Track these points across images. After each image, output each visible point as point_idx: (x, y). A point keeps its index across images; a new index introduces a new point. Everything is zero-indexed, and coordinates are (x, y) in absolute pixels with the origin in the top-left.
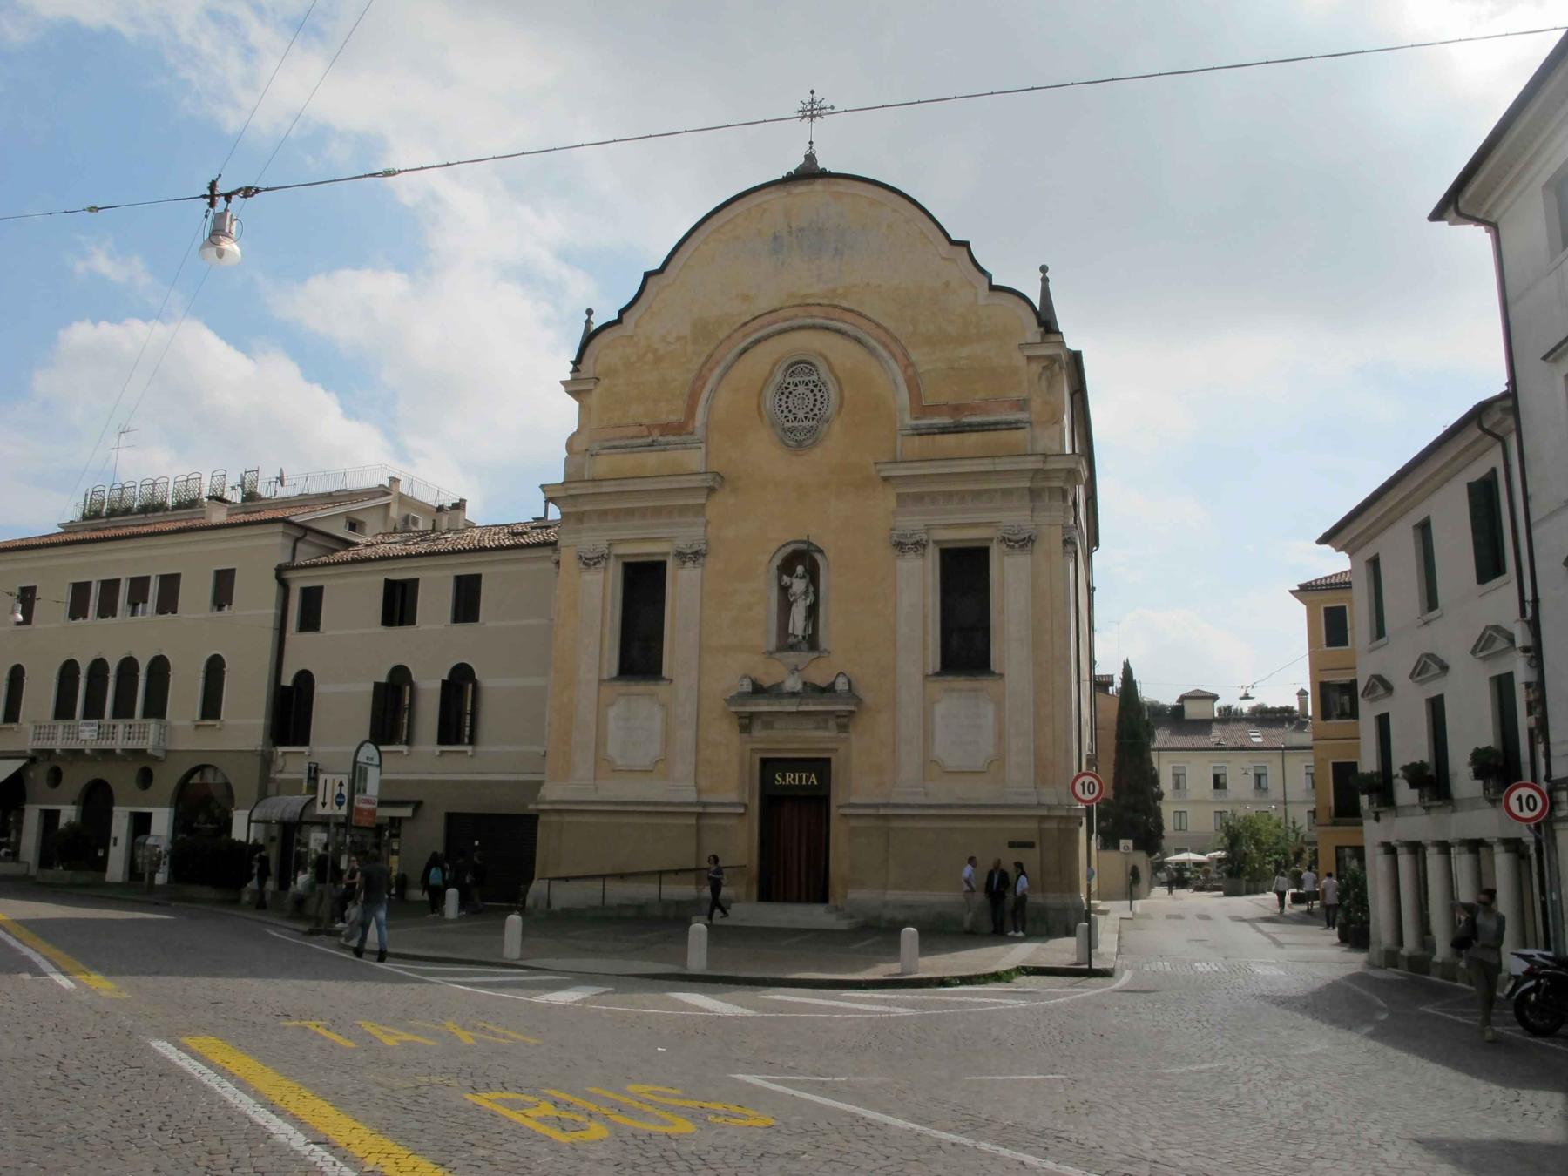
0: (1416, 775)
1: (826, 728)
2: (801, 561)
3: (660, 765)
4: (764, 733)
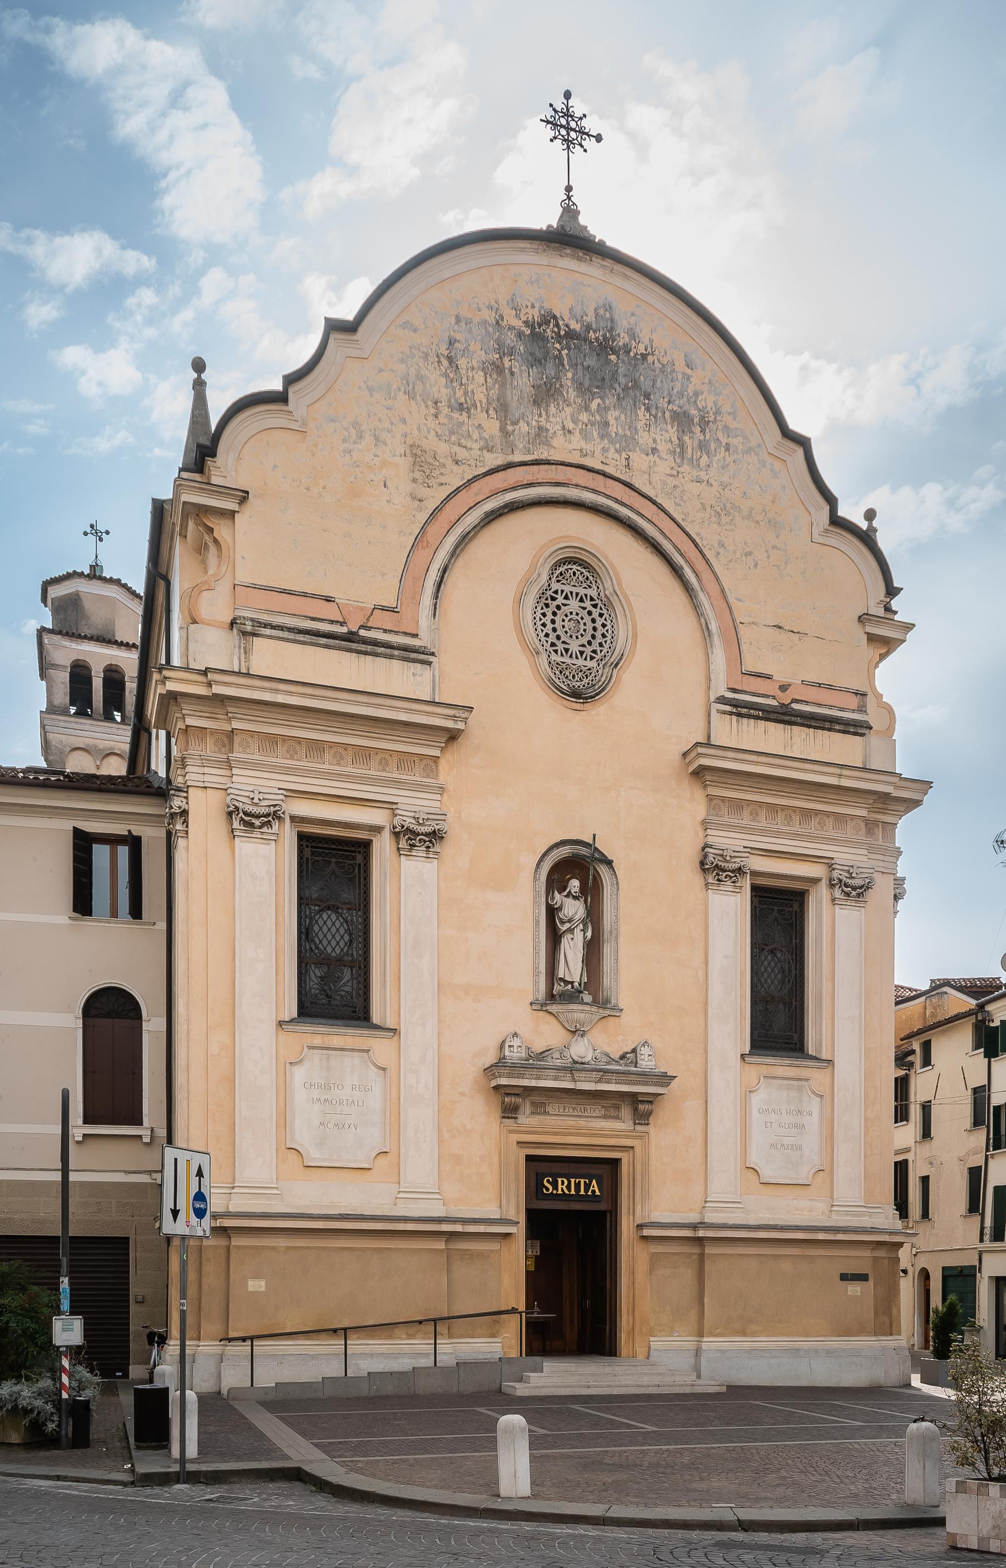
1: (617, 1118)
2: (577, 869)
3: (382, 1161)
4: (535, 1121)
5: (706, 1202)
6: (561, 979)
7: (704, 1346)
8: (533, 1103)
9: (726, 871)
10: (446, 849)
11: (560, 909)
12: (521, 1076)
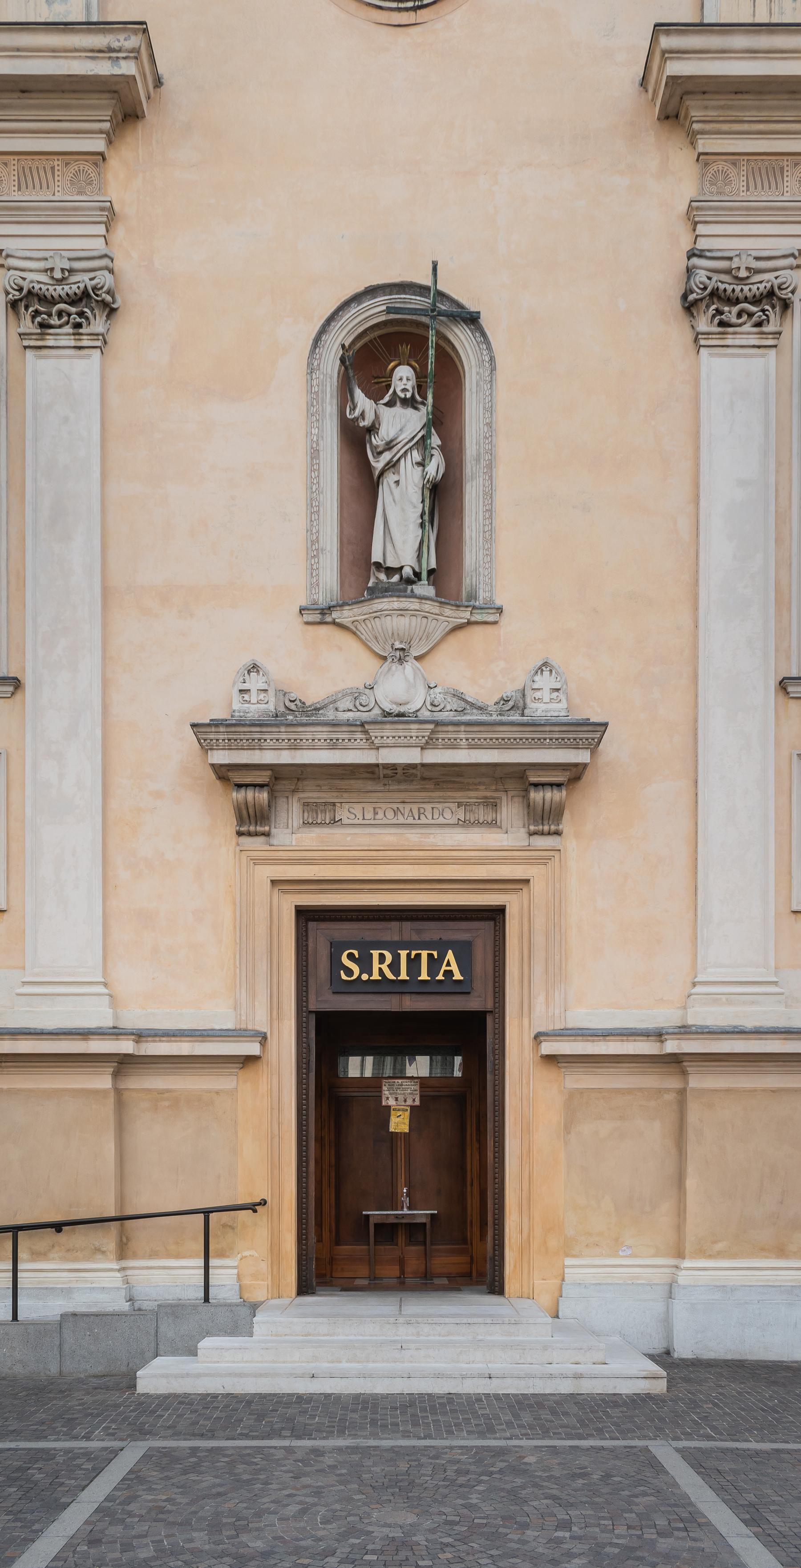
0: (431, 572)
1: (493, 824)
2: (405, 347)
5: (694, 984)
6: (378, 565)
7: (683, 1278)
8: (306, 805)
9: (737, 301)
10: (125, 333)
11: (372, 429)
12: (257, 745)
